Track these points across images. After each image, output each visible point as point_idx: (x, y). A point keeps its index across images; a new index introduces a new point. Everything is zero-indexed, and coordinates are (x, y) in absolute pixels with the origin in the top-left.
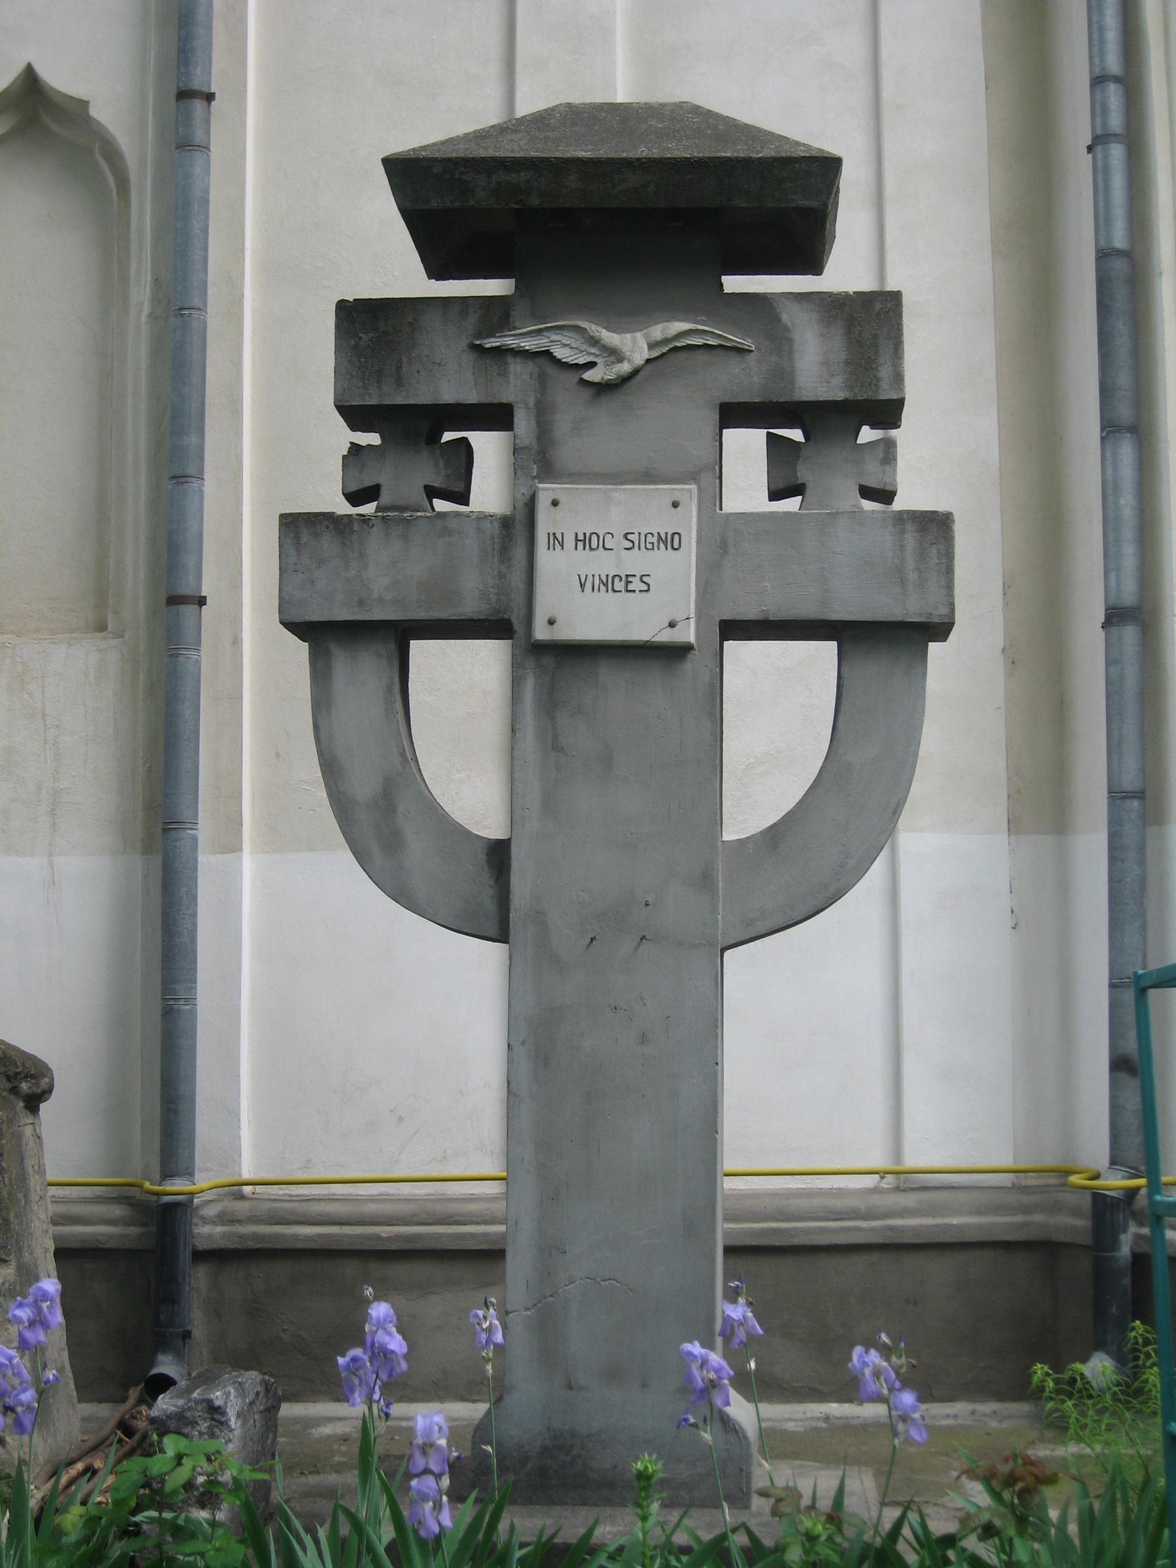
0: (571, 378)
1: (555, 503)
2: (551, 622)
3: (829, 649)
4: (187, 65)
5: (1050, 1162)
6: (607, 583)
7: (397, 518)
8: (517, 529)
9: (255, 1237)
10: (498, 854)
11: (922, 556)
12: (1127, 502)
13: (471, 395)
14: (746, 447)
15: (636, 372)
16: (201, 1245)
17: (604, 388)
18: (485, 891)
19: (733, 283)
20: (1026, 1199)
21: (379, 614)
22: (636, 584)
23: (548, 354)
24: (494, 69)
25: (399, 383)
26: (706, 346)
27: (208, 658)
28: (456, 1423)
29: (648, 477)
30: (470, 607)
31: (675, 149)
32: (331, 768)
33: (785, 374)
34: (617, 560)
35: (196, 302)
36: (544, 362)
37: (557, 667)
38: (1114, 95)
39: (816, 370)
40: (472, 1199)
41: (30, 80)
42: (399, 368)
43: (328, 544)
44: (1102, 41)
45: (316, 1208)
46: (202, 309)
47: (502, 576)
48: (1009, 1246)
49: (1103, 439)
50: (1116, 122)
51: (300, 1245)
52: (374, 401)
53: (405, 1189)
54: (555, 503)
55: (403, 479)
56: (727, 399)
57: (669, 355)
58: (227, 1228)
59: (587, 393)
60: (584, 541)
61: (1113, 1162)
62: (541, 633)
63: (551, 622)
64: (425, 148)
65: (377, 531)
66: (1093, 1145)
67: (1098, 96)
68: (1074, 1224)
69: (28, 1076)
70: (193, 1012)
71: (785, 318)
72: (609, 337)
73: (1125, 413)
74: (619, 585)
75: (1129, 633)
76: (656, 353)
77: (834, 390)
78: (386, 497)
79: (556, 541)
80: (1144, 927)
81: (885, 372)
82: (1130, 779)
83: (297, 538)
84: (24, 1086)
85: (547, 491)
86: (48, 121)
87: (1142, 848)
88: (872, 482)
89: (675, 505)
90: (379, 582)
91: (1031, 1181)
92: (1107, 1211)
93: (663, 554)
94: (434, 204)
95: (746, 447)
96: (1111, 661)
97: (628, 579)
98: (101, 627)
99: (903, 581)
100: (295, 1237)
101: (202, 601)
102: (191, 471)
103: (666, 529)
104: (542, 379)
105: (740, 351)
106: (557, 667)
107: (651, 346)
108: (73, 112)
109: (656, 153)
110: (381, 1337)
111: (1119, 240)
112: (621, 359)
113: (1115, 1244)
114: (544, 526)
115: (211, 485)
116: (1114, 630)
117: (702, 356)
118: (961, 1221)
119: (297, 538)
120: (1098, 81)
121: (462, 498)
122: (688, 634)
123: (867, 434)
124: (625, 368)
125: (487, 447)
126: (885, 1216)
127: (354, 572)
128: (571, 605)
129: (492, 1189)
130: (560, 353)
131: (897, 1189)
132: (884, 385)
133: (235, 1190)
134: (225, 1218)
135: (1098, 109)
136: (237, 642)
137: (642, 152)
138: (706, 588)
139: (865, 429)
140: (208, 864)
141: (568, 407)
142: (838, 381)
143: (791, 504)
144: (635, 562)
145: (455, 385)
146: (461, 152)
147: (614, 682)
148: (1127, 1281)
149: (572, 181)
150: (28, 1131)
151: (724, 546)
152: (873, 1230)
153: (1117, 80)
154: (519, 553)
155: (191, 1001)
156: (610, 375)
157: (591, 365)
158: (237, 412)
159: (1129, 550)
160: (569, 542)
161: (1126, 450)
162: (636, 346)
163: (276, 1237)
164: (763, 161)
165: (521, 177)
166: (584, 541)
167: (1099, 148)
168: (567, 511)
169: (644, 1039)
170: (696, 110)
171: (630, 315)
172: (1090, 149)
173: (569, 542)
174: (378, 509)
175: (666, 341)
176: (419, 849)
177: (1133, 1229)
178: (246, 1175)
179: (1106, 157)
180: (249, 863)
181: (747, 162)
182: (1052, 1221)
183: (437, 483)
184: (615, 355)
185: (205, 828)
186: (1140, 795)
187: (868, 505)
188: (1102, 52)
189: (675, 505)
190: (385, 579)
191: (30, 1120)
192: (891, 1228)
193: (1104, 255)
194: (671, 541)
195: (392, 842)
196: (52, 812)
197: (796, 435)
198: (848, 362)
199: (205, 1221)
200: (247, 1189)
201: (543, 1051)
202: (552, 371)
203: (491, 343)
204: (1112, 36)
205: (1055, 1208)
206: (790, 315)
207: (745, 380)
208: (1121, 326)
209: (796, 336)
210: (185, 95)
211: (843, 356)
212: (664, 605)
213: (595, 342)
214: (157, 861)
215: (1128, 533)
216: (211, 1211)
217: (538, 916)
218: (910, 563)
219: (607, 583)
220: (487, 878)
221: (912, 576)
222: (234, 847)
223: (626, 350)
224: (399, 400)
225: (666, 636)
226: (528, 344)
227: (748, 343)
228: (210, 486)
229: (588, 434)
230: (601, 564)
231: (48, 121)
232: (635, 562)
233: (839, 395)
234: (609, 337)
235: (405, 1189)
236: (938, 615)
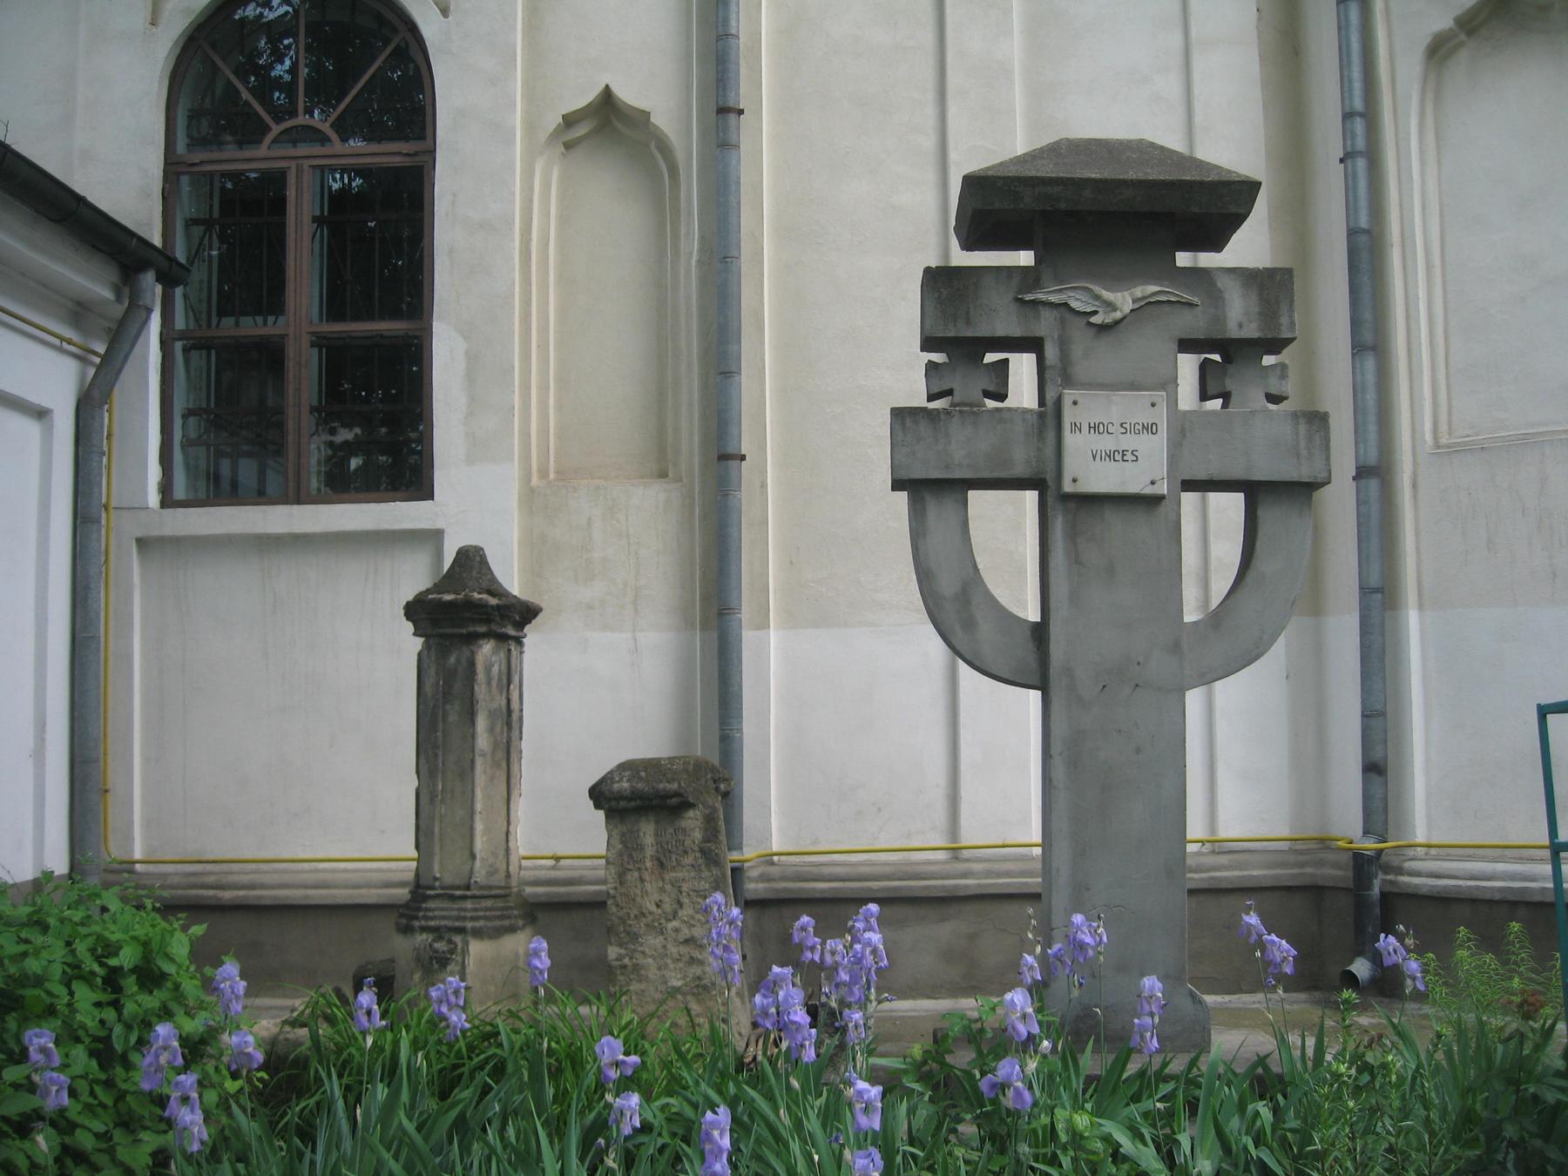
0: (1082, 321)
1: (1075, 403)
2: (1074, 481)
4: (724, 89)
5: (1311, 834)
6: (1110, 456)
7: (969, 411)
8: (1049, 416)
9: (785, 890)
10: (1255, 492)
11: (1310, 439)
12: (1371, 397)
13: (1016, 331)
14: (1188, 365)
16: (750, 896)
17: (1103, 328)
18: (1031, 659)
19: (1183, 259)
20: (1301, 858)
21: (958, 475)
22: (1129, 457)
23: (1066, 305)
24: (931, 96)
25: (968, 322)
27: (746, 497)
28: (488, 1067)
29: (1134, 386)
30: (1019, 471)
31: (1154, 174)
32: (925, 576)
33: (1220, 320)
34: (1116, 443)
35: (735, 253)
36: (1062, 309)
38: (1359, 125)
39: (1239, 315)
40: (930, 863)
41: (607, 95)
42: (968, 313)
43: (924, 428)
44: (1351, 89)
45: (826, 871)
46: (738, 258)
47: (1039, 450)
48: (1289, 889)
49: (1353, 355)
50: (1360, 143)
51: (817, 895)
52: (952, 334)
53: (883, 857)
54: (1075, 403)
55: (968, 386)
57: (1146, 307)
58: (766, 885)
59: (1094, 330)
60: (1094, 428)
61: (1366, 832)
62: (1068, 487)
63: (1074, 481)
64: (989, 168)
65: (956, 421)
66: (1347, 823)
67: (1348, 126)
68: (1340, 874)
70: (741, 738)
71: (1219, 285)
72: (1107, 295)
73: (1368, 337)
74: (1118, 457)
75: (1373, 485)
77: (1252, 331)
78: (957, 397)
79: (1076, 427)
80: (1384, 678)
81: (1284, 320)
82: (1374, 580)
83: (903, 424)
84: (722, 786)
85: (1069, 395)
86: (619, 126)
87: (1383, 624)
88: (1274, 391)
89: (1153, 405)
90: (958, 453)
91: (1299, 846)
92: (1363, 864)
93: (1145, 436)
94: (997, 206)
95: (1188, 365)
96: (1361, 502)
98: (663, 475)
99: (1298, 455)
100: (814, 890)
101: (743, 458)
102: (734, 369)
104: (1062, 321)
105: (1190, 305)
106: (1070, 511)
108: (640, 119)
109: (1141, 176)
110: (1080, 936)
111: (1363, 222)
112: (1115, 309)
113: (1370, 887)
114: (1068, 416)
115: (746, 379)
116: (1363, 481)
117: (1167, 308)
118: (1257, 874)
119: (903, 424)
120: (1348, 116)
121: (1002, 397)
122: (1163, 488)
123: (1268, 360)
124: (1118, 315)
125: (1023, 368)
126: (1209, 870)
128: (1089, 467)
129: (941, 856)
130: (1074, 304)
131: (1213, 852)
132: (1284, 328)
133: (768, 859)
134: (765, 878)
135: (1347, 134)
136: (764, 485)
137: (1131, 175)
138: (1173, 460)
139: (1265, 358)
140: (748, 637)
141: (1081, 341)
142: (1254, 325)
143: (1216, 404)
144: (1128, 442)
145: (1007, 324)
146: (1013, 172)
147: (1115, 523)
148: (1378, 911)
149: (1087, 193)
151: (1183, 431)
152: (1202, 880)
153: (1361, 115)
154: (1051, 435)
155: (740, 730)
156: (1108, 320)
157: (1095, 313)
158: (761, 329)
159: (1372, 429)
160: (1085, 428)
161: (1370, 363)
162: (1124, 300)
163: (800, 889)
164: (1212, 183)
165: (1054, 190)
166: (1094, 428)
167: (1349, 162)
168: (1081, 408)
170: (1153, 145)
171: (1118, 280)
172: (1341, 161)
173: (1085, 428)
174: (953, 405)
176: (986, 631)
177: (1381, 876)
178: (775, 848)
179: (1354, 167)
180: (774, 636)
181: (1201, 183)
182: (1318, 872)
183: (991, 388)
184: (1111, 306)
185: (746, 613)
186: (1380, 590)
187: (1271, 407)
188: (1351, 97)
189: (1153, 405)
190: (961, 450)
192: (1213, 878)
193: (1352, 233)
194: (1150, 429)
195: (969, 624)
196: (635, 602)
197: (1217, 357)
198: (1260, 314)
199: (751, 880)
200: (776, 858)
201: (1068, 763)
202: (1068, 316)
203: (1029, 297)
204: (1357, 86)
205: (1321, 863)
206: (1223, 282)
207: (1194, 324)
208: (1365, 279)
209: (1227, 296)
210: (723, 110)
211: (1257, 309)
212: (1145, 471)
213: (1097, 297)
214: (715, 635)
215: (1372, 418)
216: (754, 873)
218: (1303, 444)
219: (1110, 456)
220: (1031, 646)
221: (1304, 453)
222: (765, 625)
223: (1119, 304)
224: (969, 334)
225: (1149, 490)
226: (1053, 298)
227: (1195, 300)
228: (744, 378)
229: (1093, 358)
230: (1106, 443)
231: (619, 126)
232: (1128, 442)
233: (1255, 335)
234: (1107, 295)
235: (883, 857)
236: (1322, 476)
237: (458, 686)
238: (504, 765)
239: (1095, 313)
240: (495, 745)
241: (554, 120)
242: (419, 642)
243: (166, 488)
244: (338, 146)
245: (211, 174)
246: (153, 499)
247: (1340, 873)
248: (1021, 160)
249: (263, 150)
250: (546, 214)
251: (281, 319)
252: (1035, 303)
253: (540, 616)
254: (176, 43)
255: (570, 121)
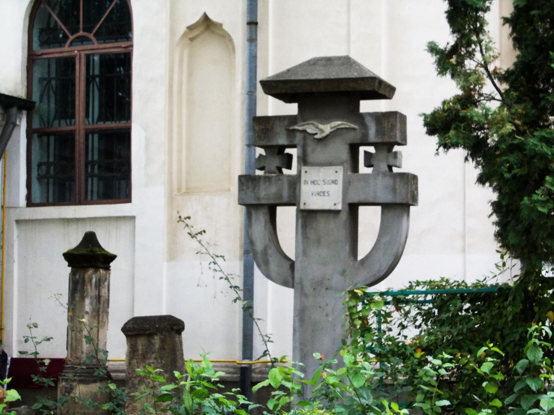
2: (305, 204)
3: (379, 208)
6: (319, 194)
10: (386, 207)
15: (327, 136)
22: (326, 194)
26: (346, 128)
29: (330, 164)
37: (307, 217)
54: (306, 172)
56: (351, 142)
63: (305, 204)
69: (175, 325)
72: (321, 126)
76: (332, 130)
79: (306, 182)
84: (175, 328)
93: (333, 186)
97: (324, 193)
103: (333, 178)
107: (332, 128)
108: (219, 26)
124: (324, 135)
127: (148, 326)
128: (311, 199)
144: (326, 188)
150: (177, 339)
157: (316, 134)
162: (327, 128)
166: (313, 182)
169: (327, 315)
171: (326, 120)
173: (309, 183)
175: (335, 127)
184: (322, 131)
189: (336, 172)
190: (266, 193)
191: (178, 336)
194: (335, 182)
203: (292, 128)
217: (301, 283)
219: (319, 194)
225: (333, 208)
226: (300, 128)
232: (326, 188)
237: (79, 287)
238: (97, 317)
239: (316, 134)
240: (94, 310)
241: (182, 29)
242: (70, 269)
243: (29, 197)
244: (96, 45)
245: (49, 59)
246: (23, 201)
247: (236, 375)
248: (273, 76)
249: (66, 48)
250: (181, 72)
251: (73, 121)
252: (294, 131)
253: (116, 259)
254: (27, 9)
255: (191, 28)
